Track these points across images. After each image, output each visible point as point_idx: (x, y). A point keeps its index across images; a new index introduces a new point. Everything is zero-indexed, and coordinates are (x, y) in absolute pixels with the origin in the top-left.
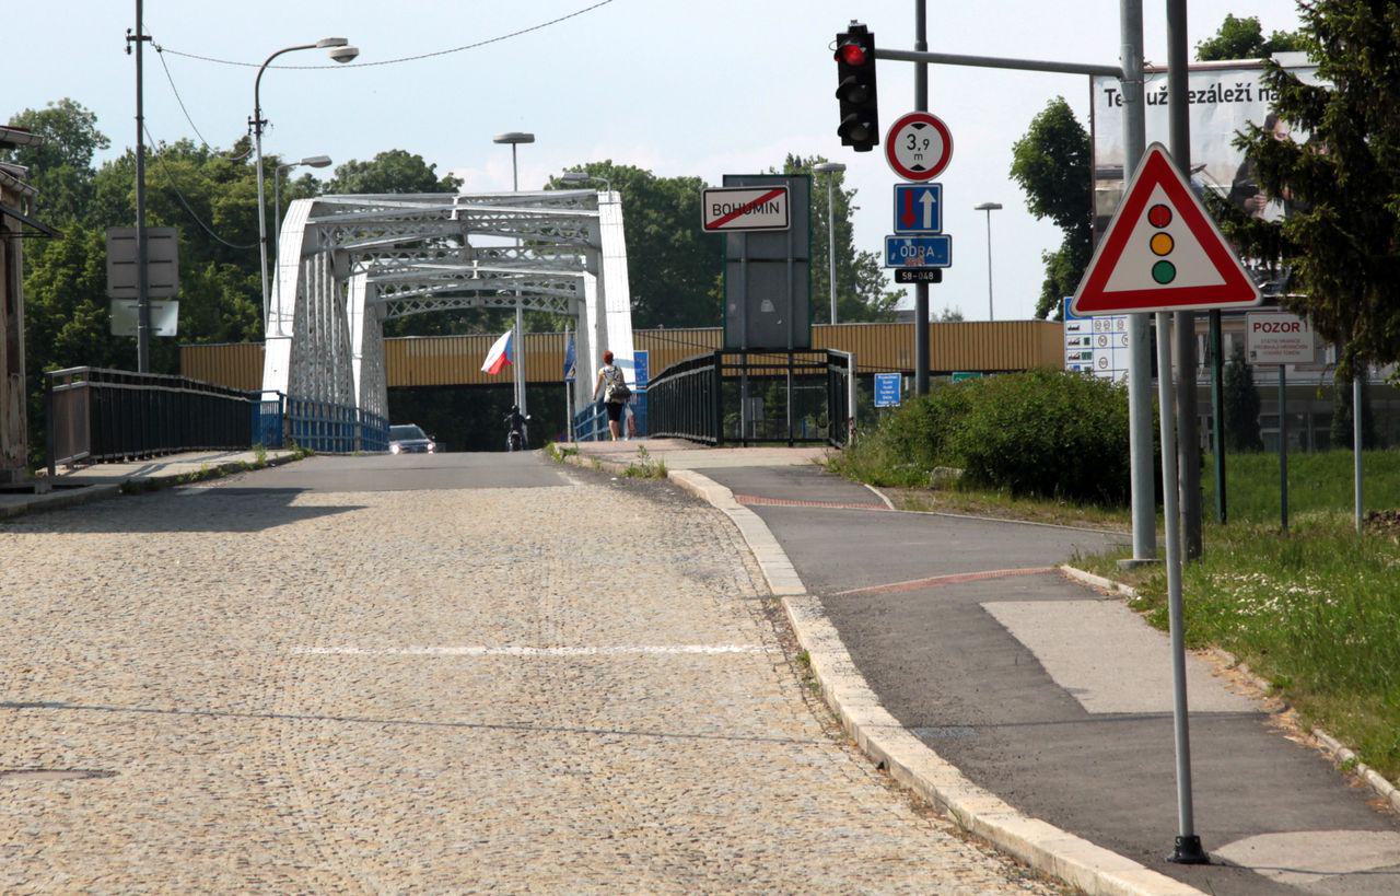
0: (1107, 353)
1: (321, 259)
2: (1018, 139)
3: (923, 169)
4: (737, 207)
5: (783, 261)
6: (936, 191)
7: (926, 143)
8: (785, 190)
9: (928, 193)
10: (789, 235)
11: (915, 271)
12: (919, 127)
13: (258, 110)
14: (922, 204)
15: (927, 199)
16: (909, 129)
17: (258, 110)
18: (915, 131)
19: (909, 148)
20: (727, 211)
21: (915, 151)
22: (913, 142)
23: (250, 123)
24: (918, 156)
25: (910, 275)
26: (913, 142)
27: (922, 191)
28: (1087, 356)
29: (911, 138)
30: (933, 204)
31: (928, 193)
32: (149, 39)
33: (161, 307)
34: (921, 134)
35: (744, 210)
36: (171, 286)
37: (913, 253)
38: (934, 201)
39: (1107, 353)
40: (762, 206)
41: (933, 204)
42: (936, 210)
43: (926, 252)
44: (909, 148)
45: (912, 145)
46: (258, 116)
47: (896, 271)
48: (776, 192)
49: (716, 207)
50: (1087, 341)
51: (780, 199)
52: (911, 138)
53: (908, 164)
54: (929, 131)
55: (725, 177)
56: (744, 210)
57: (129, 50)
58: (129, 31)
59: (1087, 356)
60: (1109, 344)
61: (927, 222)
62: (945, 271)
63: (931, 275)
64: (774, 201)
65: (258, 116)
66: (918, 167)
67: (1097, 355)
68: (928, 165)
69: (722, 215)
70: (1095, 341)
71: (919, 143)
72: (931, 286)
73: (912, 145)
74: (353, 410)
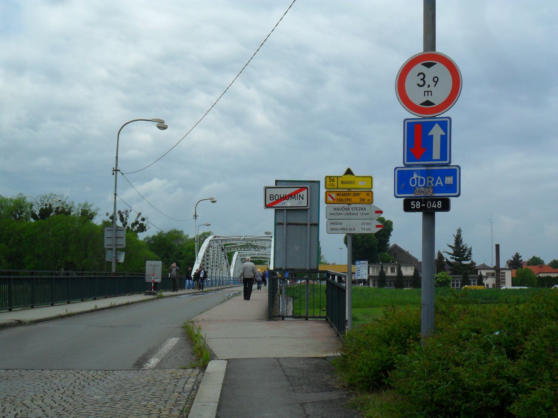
0: (362, 270)
1: (197, 243)
2: (343, 239)
3: (432, 104)
4: (282, 196)
5: (306, 225)
6: (445, 125)
7: (436, 80)
8: (307, 188)
9: (437, 126)
10: (309, 211)
11: (424, 201)
12: (429, 65)
13: (196, 213)
14: (432, 136)
15: (436, 132)
16: (419, 68)
17: (196, 213)
18: (424, 69)
19: (418, 85)
20: (277, 198)
21: (425, 88)
22: (423, 79)
23: (194, 216)
24: (427, 92)
25: (418, 204)
26: (423, 79)
27: (432, 125)
28: (359, 270)
29: (421, 76)
30: (442, 136)
31: (437, 126)
32: (119, 171)
33: (120, 254)
34: (430, 73)
35: (286, 198)
36: (123, 245)
37: (422, 183)
38: (444, 134)
39: (362, 270)
40: (295, 196)
41: (442, 136)
42: (445, 141)
43: (434, 183)
44: (418, 85)
45: (421, 83)
46: (195, 214)
47: (405, 202)
48: (302, 189)
49: (272, 196)
50: (359, 268)
51: (304, 192)
52: (421, 76)
53: (417, 98)
54: (439, 69)
55: (277, 181)
56: (286, 198)
57: (113, 174)
58: (114, 168)
59: (359, 270)
60: (363, 269)
61: (436, 153)
62: (453, 201)
63: (440, 204)
64: (301, 193)
65: (195, 214)
66: (428, 103)
67: (361, 270)
68: (438, 99)
69: (274, 200)
70: (360, 268)
71: (429, 80)
72: (437, 214)
73: (421, 83)
74: (230, 278)
